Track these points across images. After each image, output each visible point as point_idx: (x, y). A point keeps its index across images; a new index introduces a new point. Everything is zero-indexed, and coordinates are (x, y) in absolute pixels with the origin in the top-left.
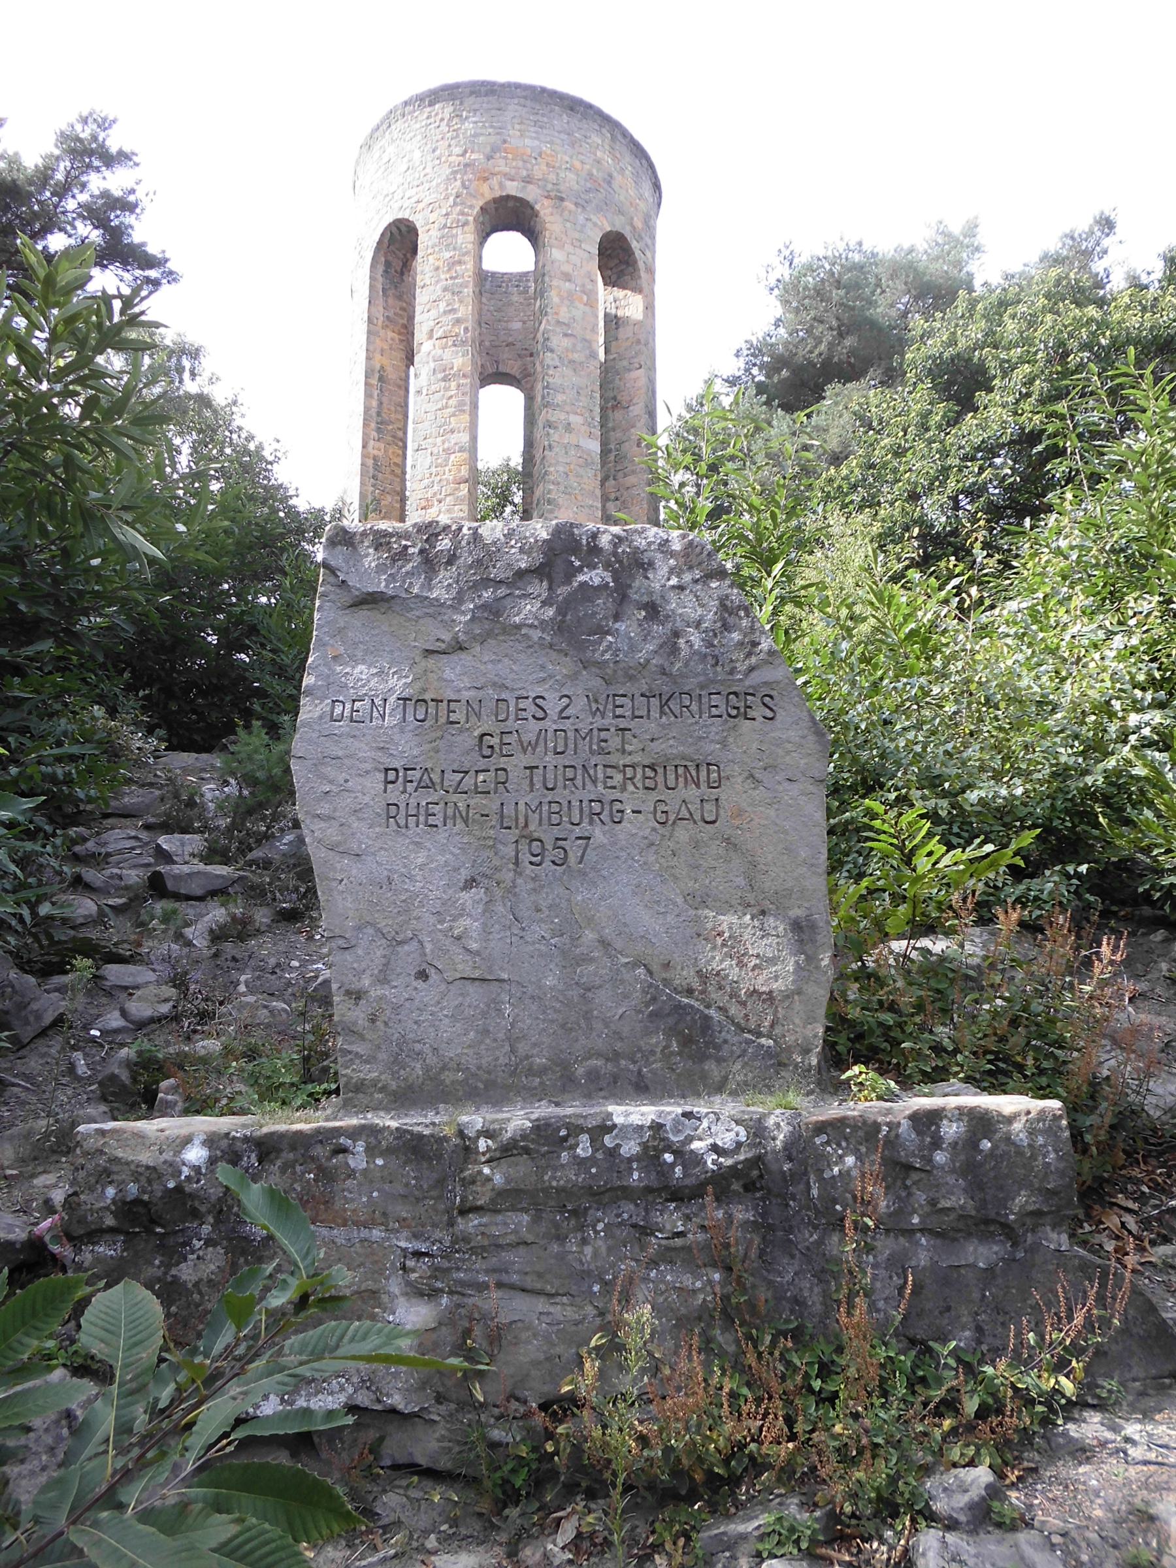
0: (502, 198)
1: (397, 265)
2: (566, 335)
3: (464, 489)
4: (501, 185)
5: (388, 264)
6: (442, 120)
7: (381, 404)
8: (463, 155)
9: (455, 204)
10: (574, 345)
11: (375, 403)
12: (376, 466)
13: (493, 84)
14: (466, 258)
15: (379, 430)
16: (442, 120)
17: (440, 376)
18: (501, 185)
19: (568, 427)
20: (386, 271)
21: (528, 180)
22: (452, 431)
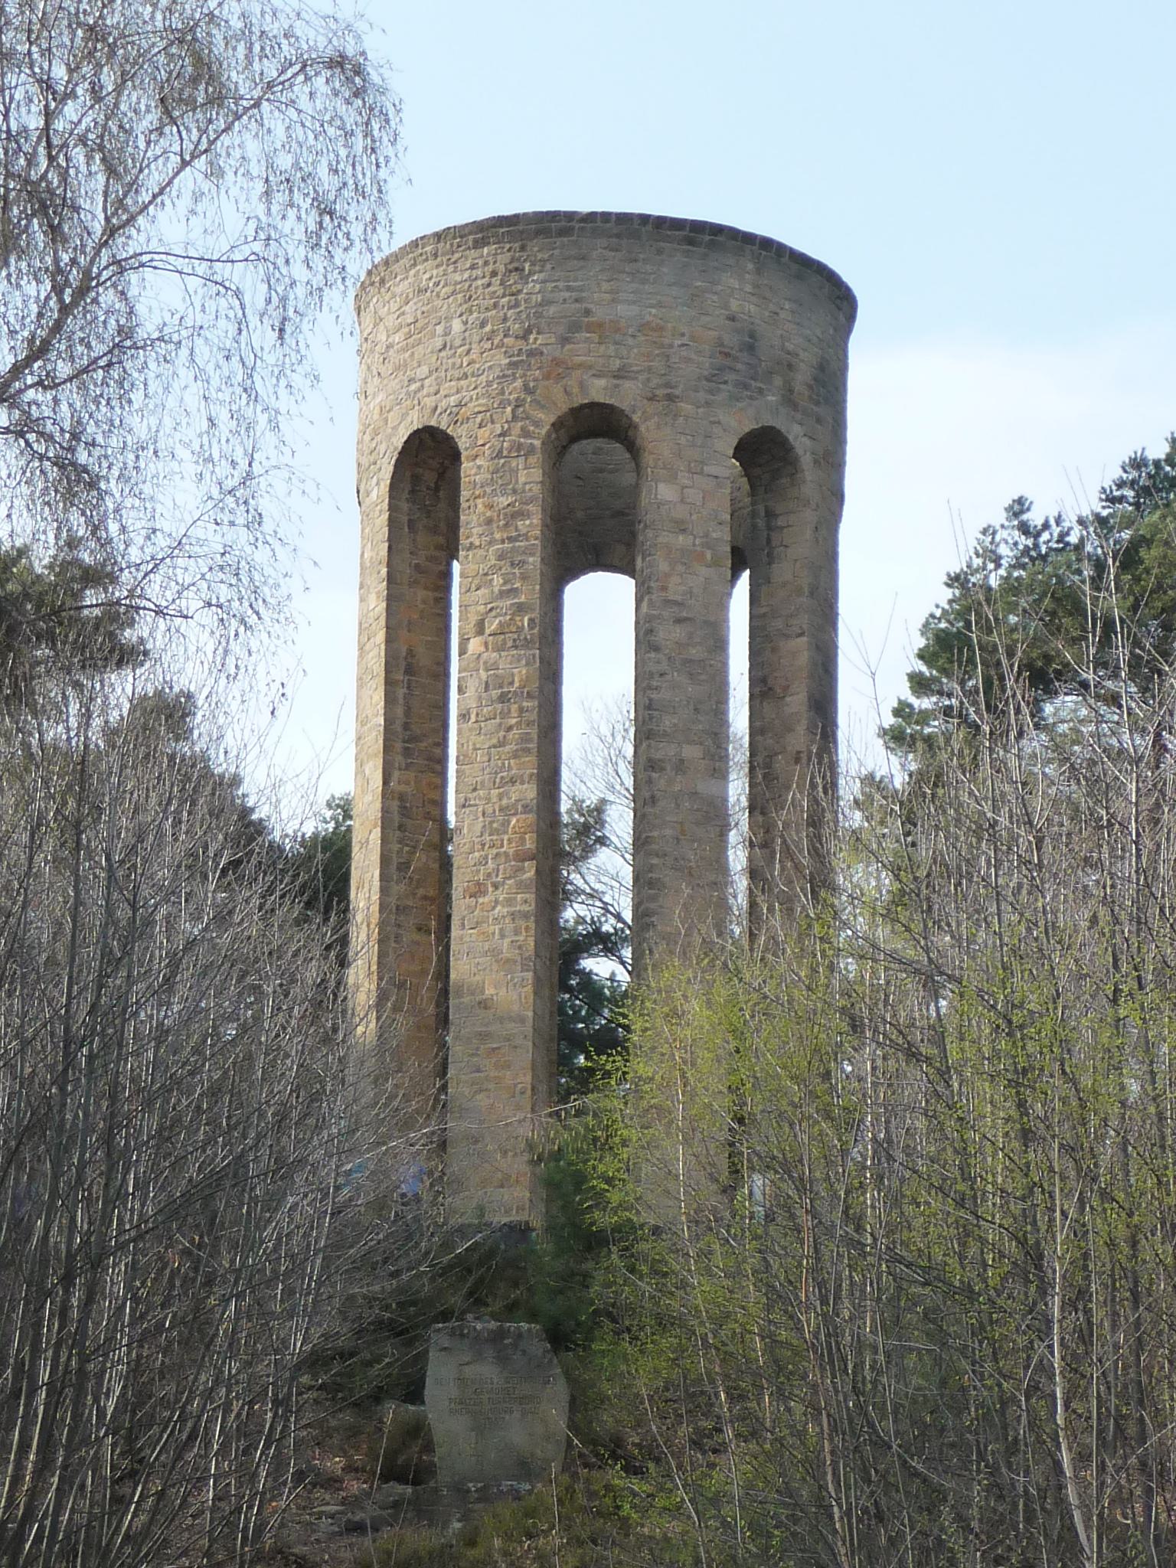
0: (582, 407)
1: (430, 477)
2: (679, 621)
3: (530, 872)
4: (582, 385)
5: (416, 479)
6: (494, 274)
7: (408, 712)
8: (525, 337)
9: (515, 418)
10: (690, 636)
11: (400, 711)
12: (404, 811)
13: (570, 216)
14: (530, 507)
15: (407, 752)
16: (494, 274)
17: (495, 693)
18: (582, 385)
19: (681, 766)
20: (413, 492)
21: (621, 374)
22: (513, 781)
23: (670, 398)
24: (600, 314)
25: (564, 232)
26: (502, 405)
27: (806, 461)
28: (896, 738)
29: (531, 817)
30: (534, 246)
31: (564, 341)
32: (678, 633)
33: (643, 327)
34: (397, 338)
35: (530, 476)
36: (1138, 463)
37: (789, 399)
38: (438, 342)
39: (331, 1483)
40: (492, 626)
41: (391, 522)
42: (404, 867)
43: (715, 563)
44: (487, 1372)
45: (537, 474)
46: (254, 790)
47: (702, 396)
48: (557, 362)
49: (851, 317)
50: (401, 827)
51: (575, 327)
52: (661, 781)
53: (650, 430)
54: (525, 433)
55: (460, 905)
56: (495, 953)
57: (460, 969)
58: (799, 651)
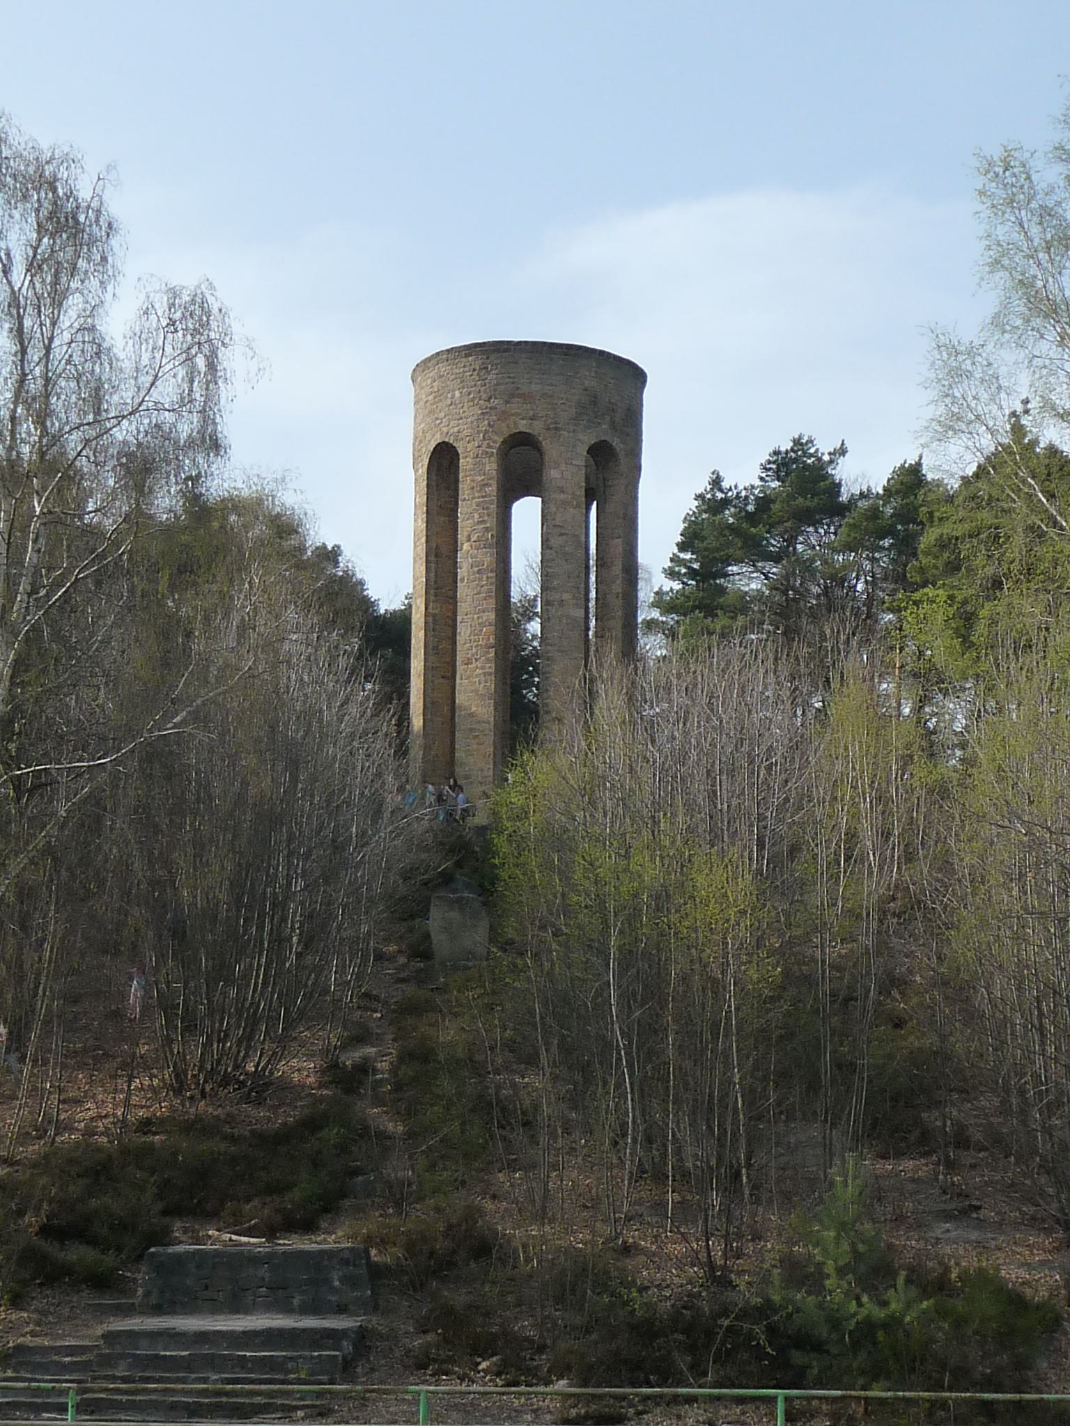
11: (432, 575)
23: (556, 429)
24: (524, 389)
25: (506, 351)
26: (478, 432)
27: (622, 455)
28: (671, 574)
29: (493, 628)
30: (492, 357)
31: (507, 402)
32: (560, 540)
33: (544, 395)
34: (431, 398)
35: (491, 467)
36: (776, 453)
37: (613, 425)
38: (449, 402)
39: (391, 958)
40: (474, 538)
41: (428, 486)
42: (436, 648)
43: (578, 506)
44: (454, 915)
45: (495, 466)
46: (372, 592)
47: (572, 428)
48: (504, 412)
49: (645, 382)
50: (434, 630)
51: (512, 396)
52: (552, 610)
53: (546, 445)
54: (489, 446)
55: (460, 668)
56: (477, 691)
57: (460, 698)
58: (617, 545)
